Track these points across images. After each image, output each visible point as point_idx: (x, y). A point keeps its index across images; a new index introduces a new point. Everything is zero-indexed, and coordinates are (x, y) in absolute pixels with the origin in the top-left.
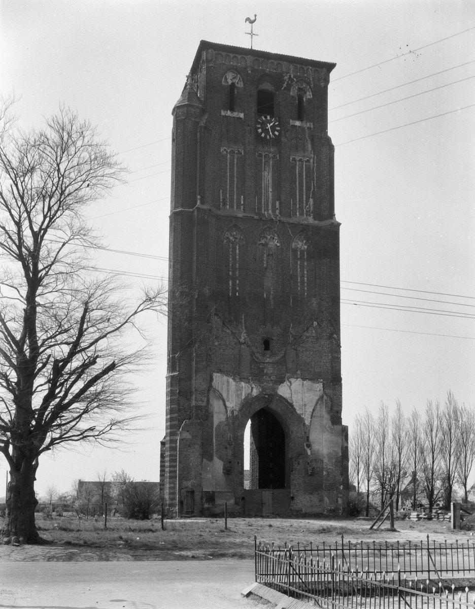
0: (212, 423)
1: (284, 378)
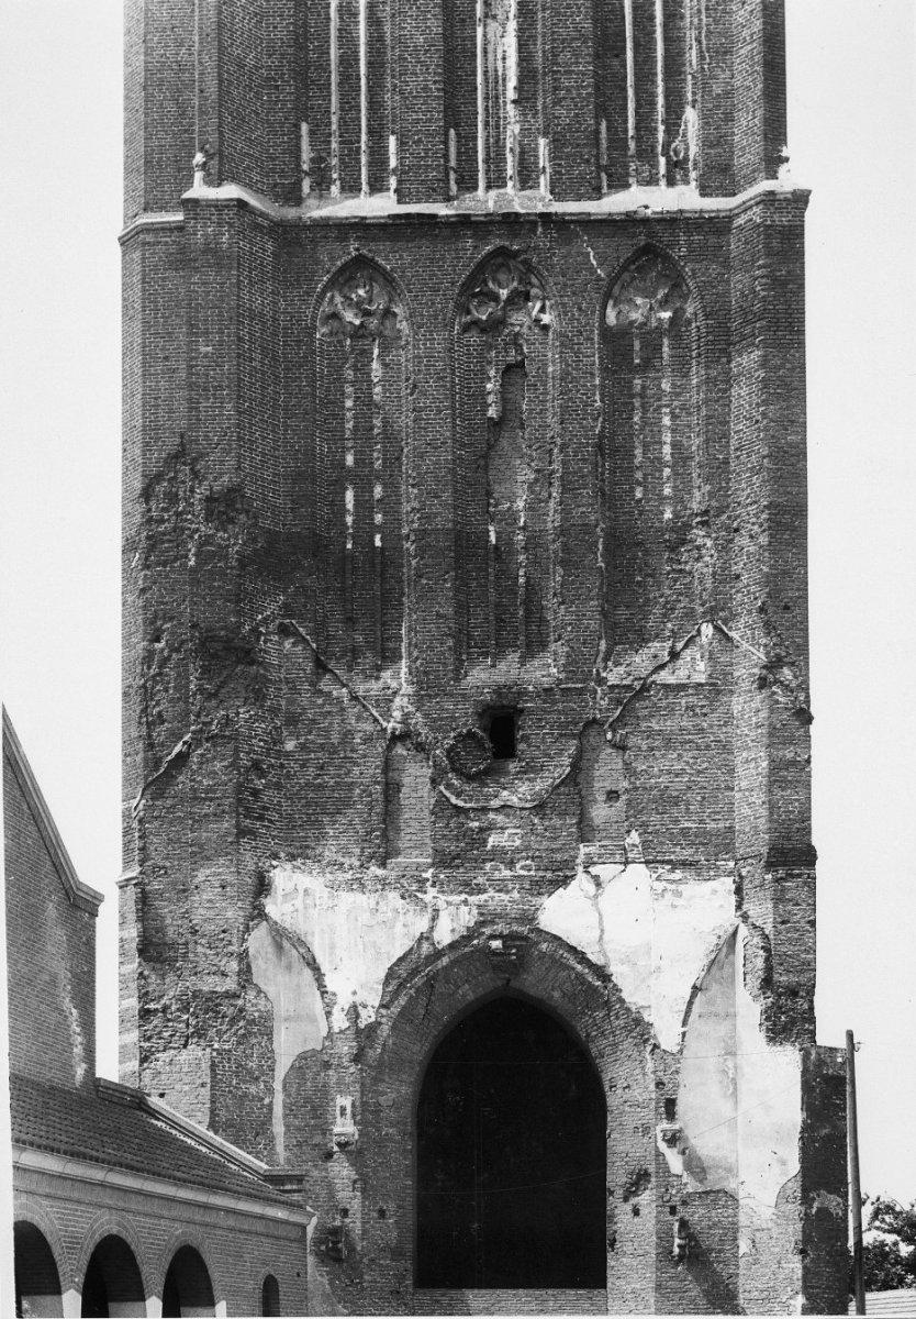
0: (269, 1056)
1: (569, 864)
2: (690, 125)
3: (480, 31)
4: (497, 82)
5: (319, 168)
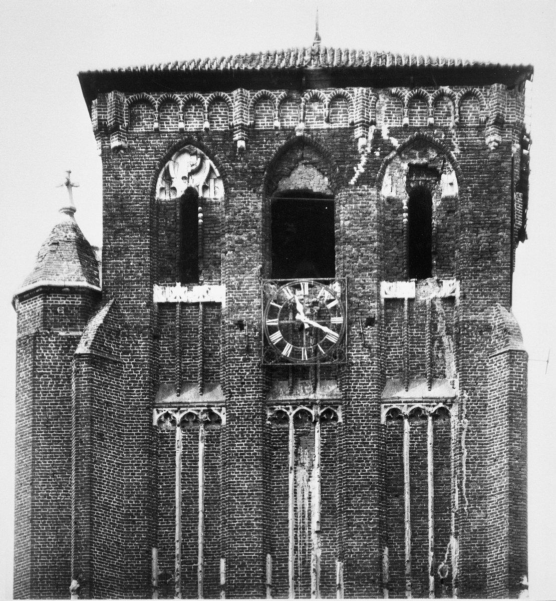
2: (453, 551)
3: (291, 476)
4: (304, 517)
5: (165, 583)
